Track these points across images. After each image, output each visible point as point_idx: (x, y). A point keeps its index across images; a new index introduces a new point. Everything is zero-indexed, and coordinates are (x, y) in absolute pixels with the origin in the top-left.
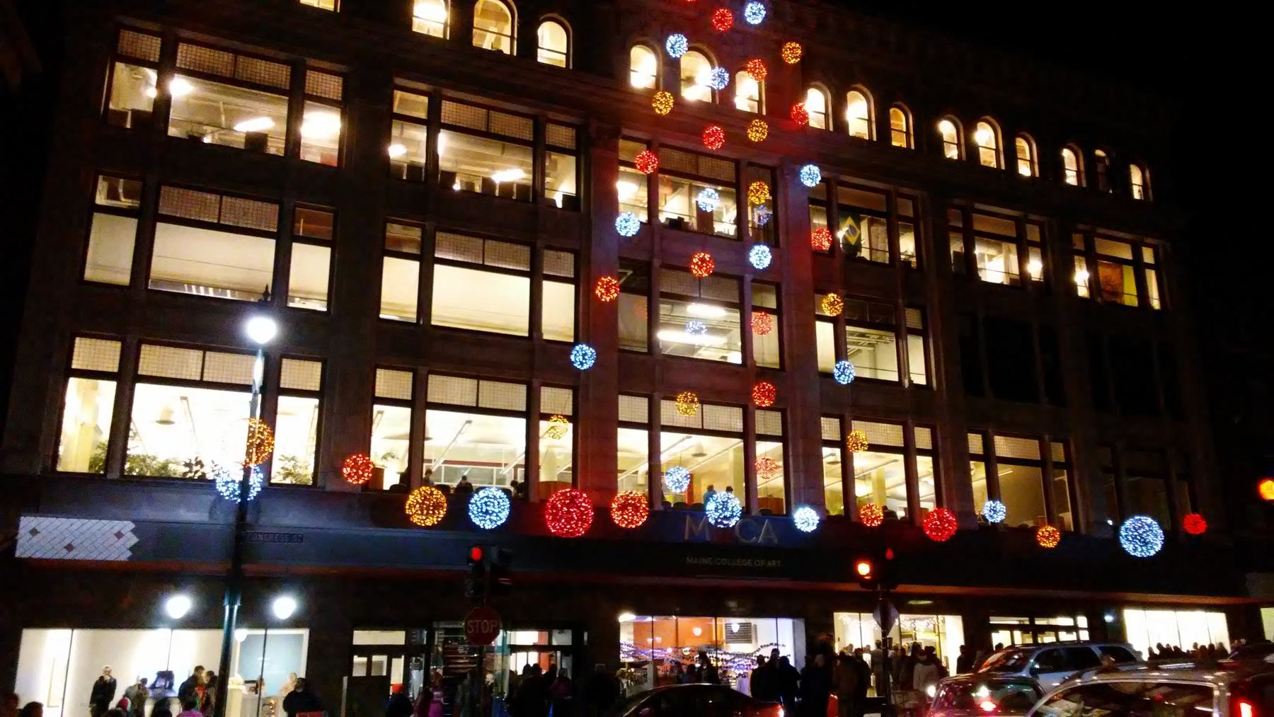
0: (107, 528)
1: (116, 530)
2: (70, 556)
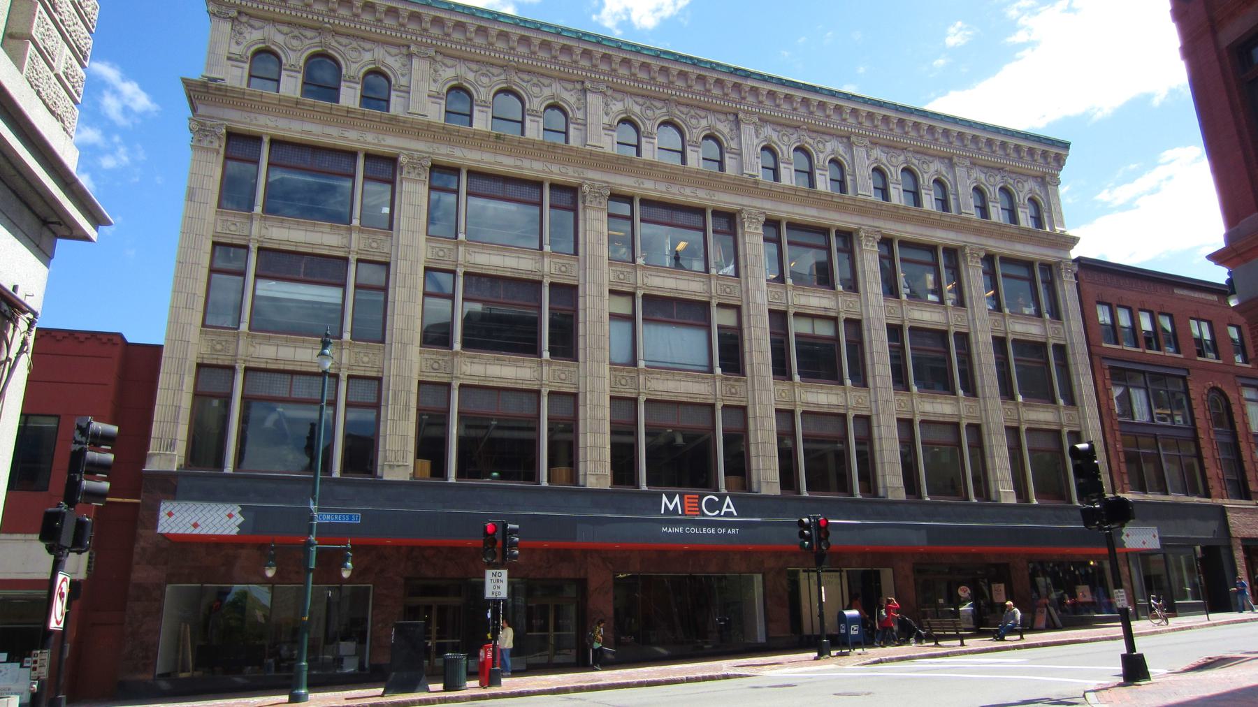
2: (197, 531)
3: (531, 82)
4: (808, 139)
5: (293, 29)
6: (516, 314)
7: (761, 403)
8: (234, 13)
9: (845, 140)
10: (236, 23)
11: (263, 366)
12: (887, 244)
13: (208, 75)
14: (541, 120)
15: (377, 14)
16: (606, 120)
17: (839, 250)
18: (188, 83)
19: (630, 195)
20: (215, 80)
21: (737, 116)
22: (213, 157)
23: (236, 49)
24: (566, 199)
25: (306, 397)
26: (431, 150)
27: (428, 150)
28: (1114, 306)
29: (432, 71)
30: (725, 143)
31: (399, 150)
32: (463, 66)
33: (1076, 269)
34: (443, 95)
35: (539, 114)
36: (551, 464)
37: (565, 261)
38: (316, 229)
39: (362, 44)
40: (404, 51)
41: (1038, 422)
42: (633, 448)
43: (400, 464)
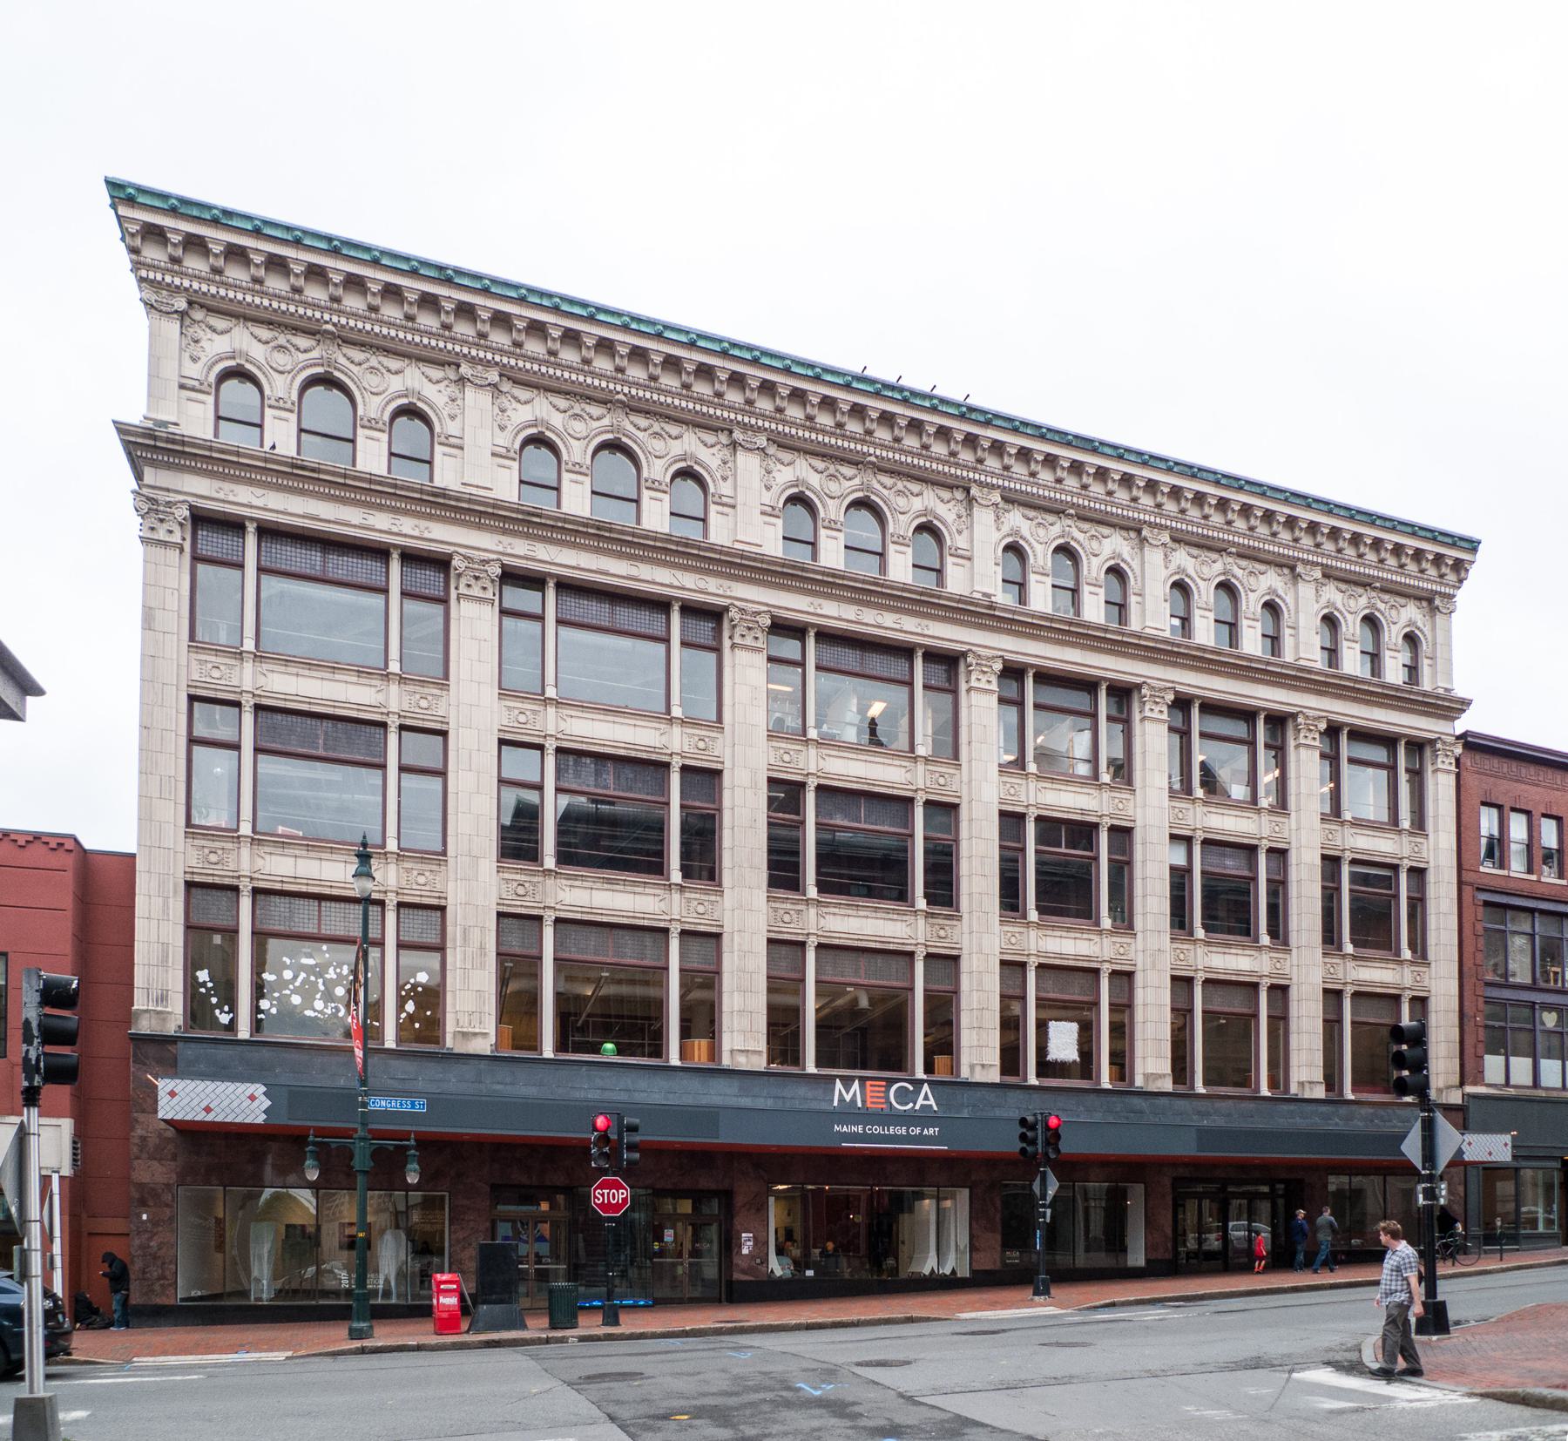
0: (240, 1090)
1: (248, 1093)
2: (210, 1118)
3: (570, 413)
4: (1077, 534)
5: (368, 356)
6: (860, 839)
7: (980, 952)
8: (181, 304)
9: (1425, 604)
10: (187, 321)
11: (278, 886)
12: (1182, 709)
13: (153, 416)
14: (666, 497)
15: (292, 277)
16: (768, 498)
17: (1110, 719)
18: (122, 429)
19: (801, 626)
20: (165, 424)
21: (968, 492)
22: (173, 555)
23: (194, 371)
24: (704, 629)
25: (342, 933)
26: (500, 549)
27: (495, 548)
28: (1507, 809)
29: (497, 410)
30: (948, 538)
31: (729, 601)
32: (931, 492)
33: (1459, 750)
34: (293, 404)
35: (663, 487)
36: (686, 1033)
37: (704, 733)
38: (337, 677)
39: (386, 361)
40: (724, 438)
41: (1372, 983)
42: (796, 1013)
43: (477, 1030)
